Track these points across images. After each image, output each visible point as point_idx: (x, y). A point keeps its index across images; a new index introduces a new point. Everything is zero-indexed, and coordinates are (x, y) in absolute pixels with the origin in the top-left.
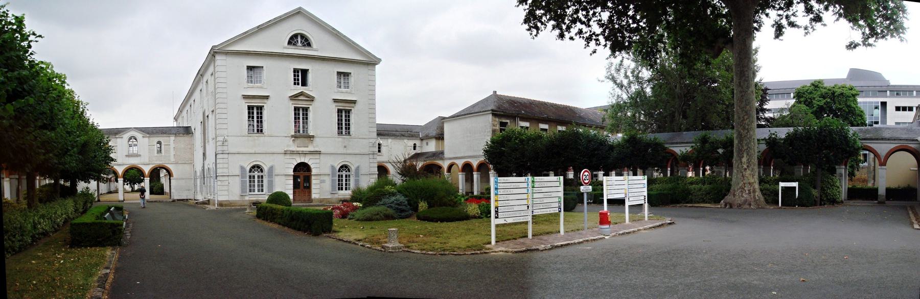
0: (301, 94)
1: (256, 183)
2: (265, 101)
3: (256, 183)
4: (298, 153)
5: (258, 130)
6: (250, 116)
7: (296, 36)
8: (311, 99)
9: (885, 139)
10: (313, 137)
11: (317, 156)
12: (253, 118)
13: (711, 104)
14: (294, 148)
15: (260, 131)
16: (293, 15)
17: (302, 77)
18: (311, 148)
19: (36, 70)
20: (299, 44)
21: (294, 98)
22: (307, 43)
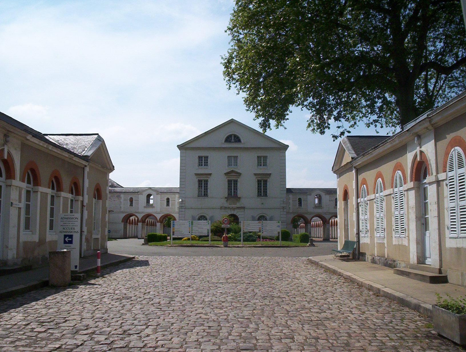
0: (232, 171)
1: (203, 161)
2: (209, 177)
3: (203, 161)
4: (229, 208)
5: (204, 194)
6: (200, 186)
7: (230, 136)
8: (239, 174)
9: (14, 271)
10: (240, 198)
11: (242, 210)
12: (202, 187)
13: (347, 318)
14: (226, 205)
15: (206, 195)
16: (229, 123)
17: (232, 160)
18: (238, 205)
19: (159, 236)
20: (233, 141)
21: (227, 174)
22: (237, 139)
